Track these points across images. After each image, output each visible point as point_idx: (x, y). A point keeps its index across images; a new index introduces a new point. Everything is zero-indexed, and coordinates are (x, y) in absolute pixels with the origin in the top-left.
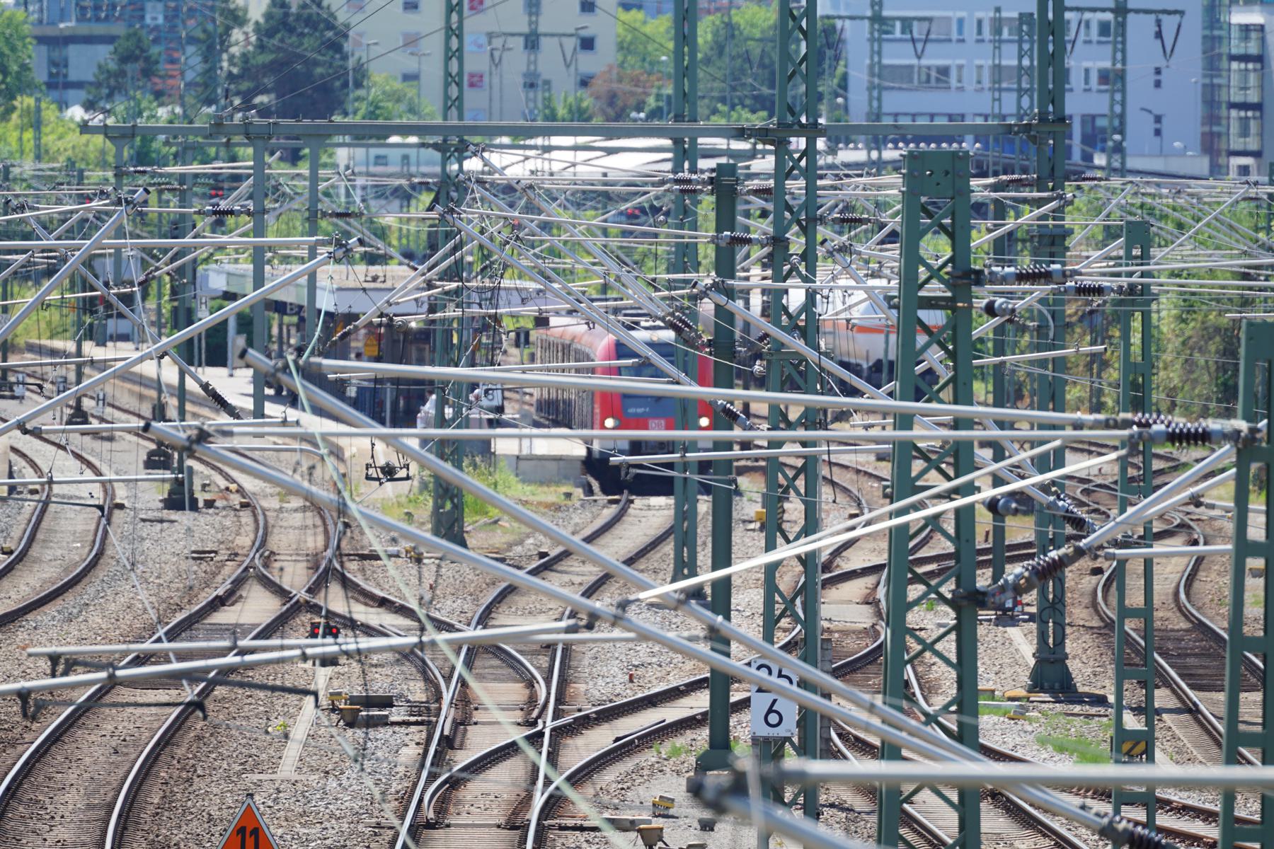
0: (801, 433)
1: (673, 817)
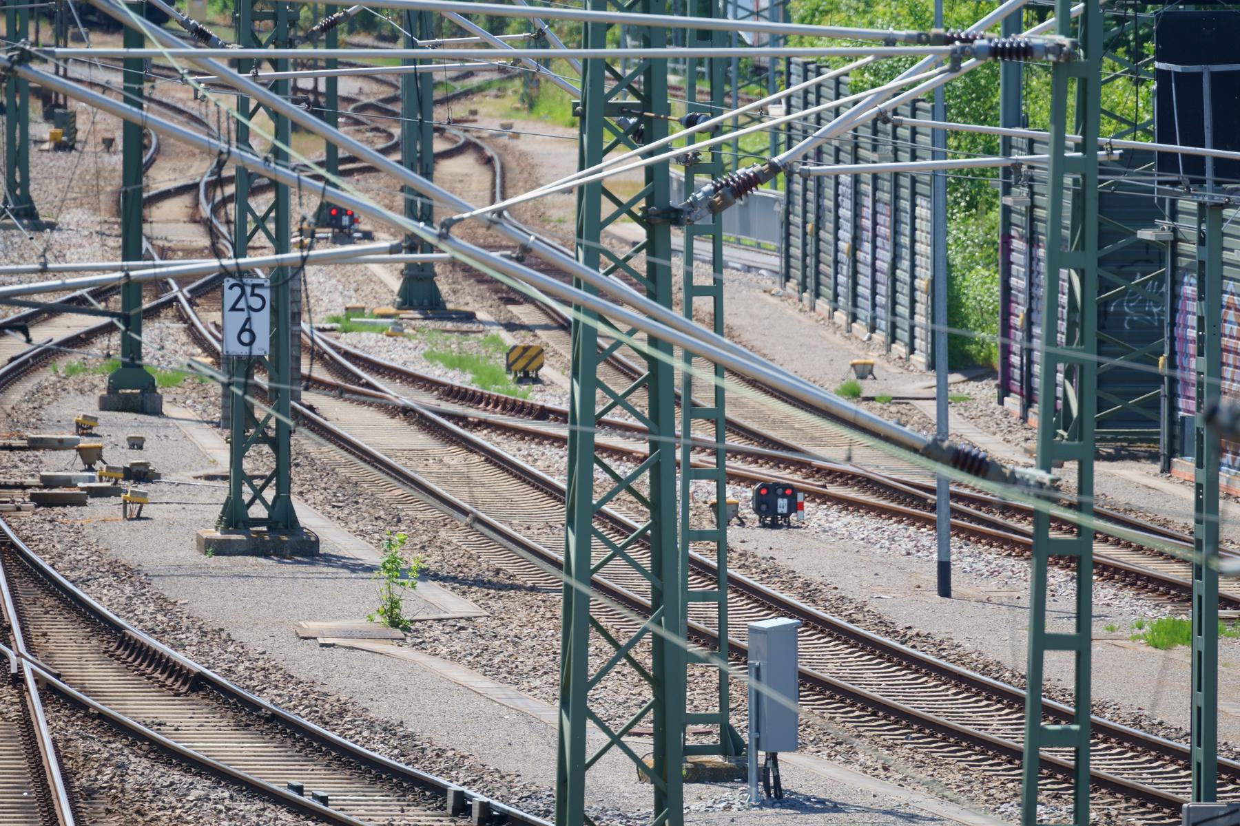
0: (272, 50)
1: (96, 435)
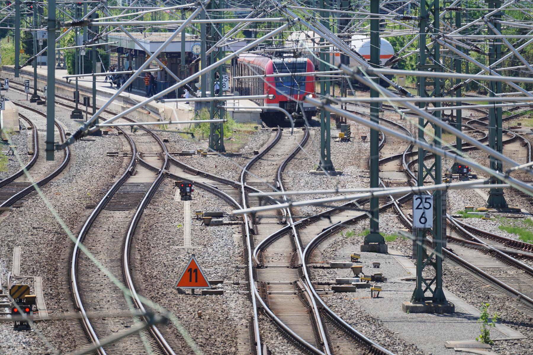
0: (433, 98)
1: (359, 262)
